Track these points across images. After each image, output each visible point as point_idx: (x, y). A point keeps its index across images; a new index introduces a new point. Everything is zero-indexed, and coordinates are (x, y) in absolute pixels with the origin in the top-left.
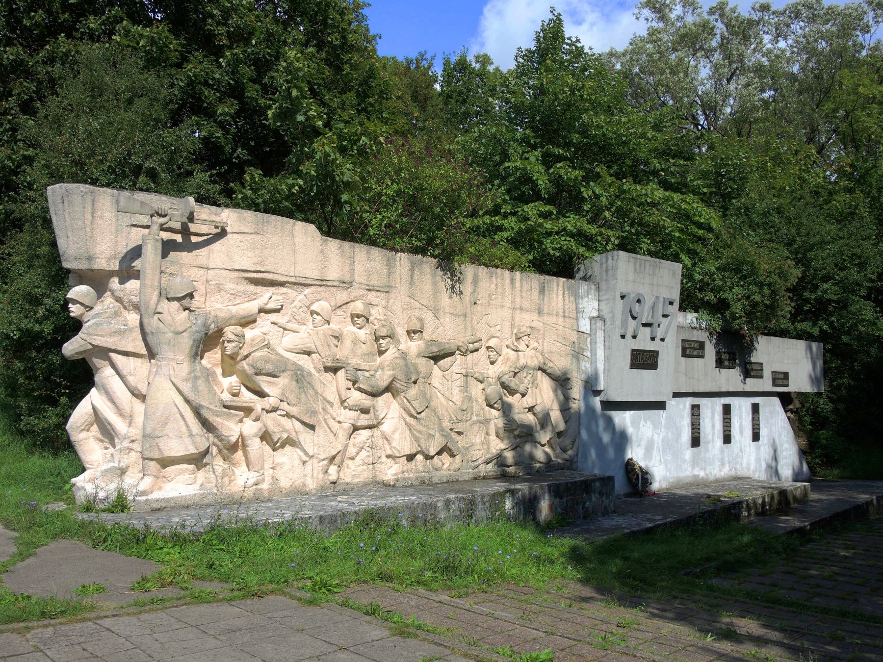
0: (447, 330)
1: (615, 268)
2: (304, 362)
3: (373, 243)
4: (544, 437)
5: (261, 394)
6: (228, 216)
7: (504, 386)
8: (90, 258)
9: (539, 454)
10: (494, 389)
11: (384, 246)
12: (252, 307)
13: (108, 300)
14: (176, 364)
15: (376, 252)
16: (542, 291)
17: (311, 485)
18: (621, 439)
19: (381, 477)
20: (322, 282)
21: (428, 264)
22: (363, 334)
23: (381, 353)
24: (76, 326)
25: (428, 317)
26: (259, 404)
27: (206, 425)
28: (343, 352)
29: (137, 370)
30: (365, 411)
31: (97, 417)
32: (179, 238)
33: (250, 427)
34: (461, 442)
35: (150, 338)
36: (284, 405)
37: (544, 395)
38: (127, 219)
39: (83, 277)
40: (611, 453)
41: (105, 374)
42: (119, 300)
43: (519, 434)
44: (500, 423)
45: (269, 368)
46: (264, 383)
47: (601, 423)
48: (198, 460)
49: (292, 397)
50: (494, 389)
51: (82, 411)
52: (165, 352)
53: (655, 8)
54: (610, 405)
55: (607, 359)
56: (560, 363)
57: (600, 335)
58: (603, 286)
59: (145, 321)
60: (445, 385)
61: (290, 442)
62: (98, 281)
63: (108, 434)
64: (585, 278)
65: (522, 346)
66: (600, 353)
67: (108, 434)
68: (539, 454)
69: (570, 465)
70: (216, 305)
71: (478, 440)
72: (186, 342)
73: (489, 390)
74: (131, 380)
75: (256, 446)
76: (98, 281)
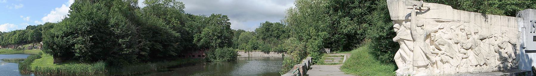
0: (484, 33)
1: (529, 14)
2: (450, 41)
3: (464, 10)
4: (510, 60)
5: (440, 50)
6: (430, 5)
7: (499, 46)
8: (398, 17)
9: (509, 65)
10: (497, 48)
11: (467, 10)
12: (437, 28)
13: (402, 27)
14: (420, 42)
15: (466, 12)
16: (508, 21)
17: (453, 73)
18: (531, 61)
19: (469, 71)
20: (453, 21)
21: (479, 15)
22: (464, 34)
23: (468, 39)
24: (395, 34)
25: (479, 29)
26: (440, 52)
27: (427, 57)
28: (459, 39)
29: (410, 44)
30: (465, 54)
31: (401, 56)
32: (419, 11)
33: (438, 58)
34: (488, 62)
35: (414, 36)
36: (446, 53)
37: (510, 49)
38: (407, 7)
39: (396, 22)
40: (528, 65)
41: (402, 45)
42: (405, 27)
43: (504, 60)
44: (499, 57)
45: (442, 43)
46: (441, 47)
47: (525, 57)
48: (426, 67)
49: (448, 51)
50: (497, 48)
51: (397, 55)
52: (418, 40)
53: (35, 41)
54: (527, 51)
55: (527, 39)
56: (513, 42)
57: (525, 32)
58: (525, 18)
59: (413, 32)
60: (484, 46)
61: (447, 62)
62: (400, 22)
63: (404, 60)
64: (520, 17)
65: (504, 36)
66: (525, 37)
67: (404, 60)
68: (509, 65)
69: (517, 67)
70: (430, 27)
71: (493, 61)
72: (423, 37)
73: (495, 48)
74: (409, 47)
75: (439, 63)
76: (400, 22)
